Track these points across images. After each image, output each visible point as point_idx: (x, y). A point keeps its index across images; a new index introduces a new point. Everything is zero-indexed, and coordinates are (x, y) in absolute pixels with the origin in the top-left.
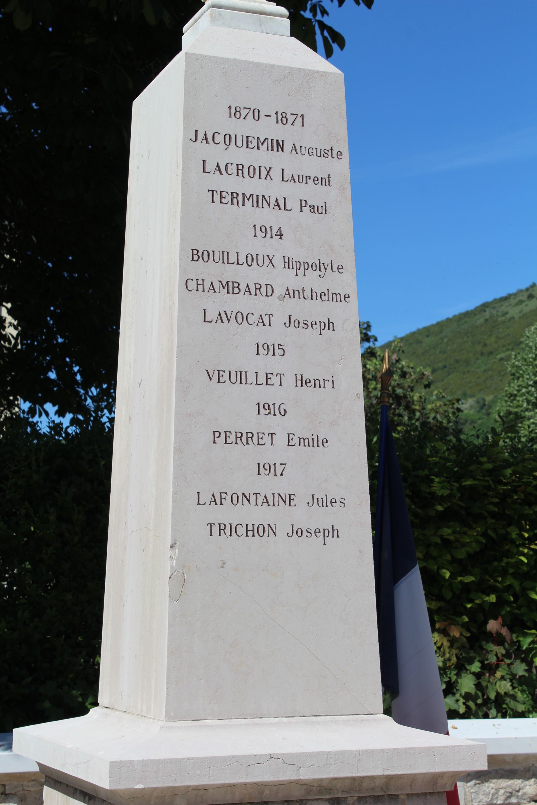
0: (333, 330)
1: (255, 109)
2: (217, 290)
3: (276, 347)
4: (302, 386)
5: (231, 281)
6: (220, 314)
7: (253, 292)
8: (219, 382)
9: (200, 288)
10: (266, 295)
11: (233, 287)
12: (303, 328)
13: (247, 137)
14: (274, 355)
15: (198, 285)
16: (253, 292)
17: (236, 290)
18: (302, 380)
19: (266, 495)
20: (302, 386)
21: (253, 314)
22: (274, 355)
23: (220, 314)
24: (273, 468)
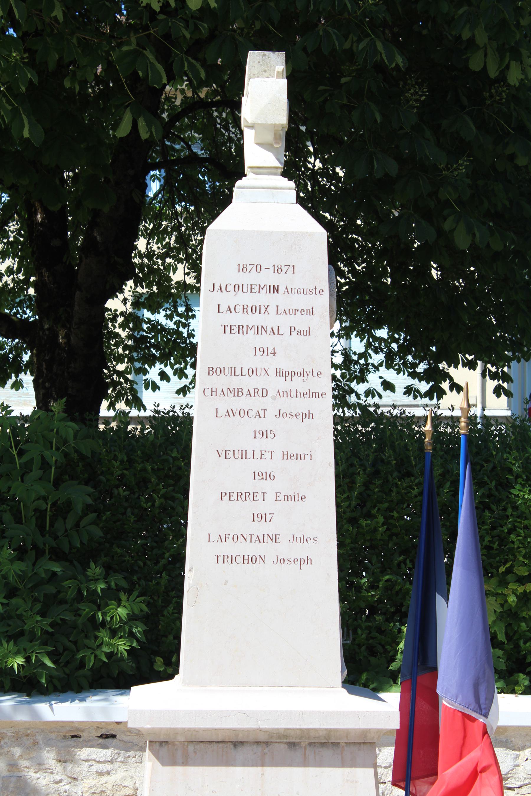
2: (226, 394)
4: (287, 459)
7: (252, 394)
9: (214, 393)
11: (238, 392)
16: (252, 394)
17: (240, 394)
18: (287, 455)
22: (267, 437)
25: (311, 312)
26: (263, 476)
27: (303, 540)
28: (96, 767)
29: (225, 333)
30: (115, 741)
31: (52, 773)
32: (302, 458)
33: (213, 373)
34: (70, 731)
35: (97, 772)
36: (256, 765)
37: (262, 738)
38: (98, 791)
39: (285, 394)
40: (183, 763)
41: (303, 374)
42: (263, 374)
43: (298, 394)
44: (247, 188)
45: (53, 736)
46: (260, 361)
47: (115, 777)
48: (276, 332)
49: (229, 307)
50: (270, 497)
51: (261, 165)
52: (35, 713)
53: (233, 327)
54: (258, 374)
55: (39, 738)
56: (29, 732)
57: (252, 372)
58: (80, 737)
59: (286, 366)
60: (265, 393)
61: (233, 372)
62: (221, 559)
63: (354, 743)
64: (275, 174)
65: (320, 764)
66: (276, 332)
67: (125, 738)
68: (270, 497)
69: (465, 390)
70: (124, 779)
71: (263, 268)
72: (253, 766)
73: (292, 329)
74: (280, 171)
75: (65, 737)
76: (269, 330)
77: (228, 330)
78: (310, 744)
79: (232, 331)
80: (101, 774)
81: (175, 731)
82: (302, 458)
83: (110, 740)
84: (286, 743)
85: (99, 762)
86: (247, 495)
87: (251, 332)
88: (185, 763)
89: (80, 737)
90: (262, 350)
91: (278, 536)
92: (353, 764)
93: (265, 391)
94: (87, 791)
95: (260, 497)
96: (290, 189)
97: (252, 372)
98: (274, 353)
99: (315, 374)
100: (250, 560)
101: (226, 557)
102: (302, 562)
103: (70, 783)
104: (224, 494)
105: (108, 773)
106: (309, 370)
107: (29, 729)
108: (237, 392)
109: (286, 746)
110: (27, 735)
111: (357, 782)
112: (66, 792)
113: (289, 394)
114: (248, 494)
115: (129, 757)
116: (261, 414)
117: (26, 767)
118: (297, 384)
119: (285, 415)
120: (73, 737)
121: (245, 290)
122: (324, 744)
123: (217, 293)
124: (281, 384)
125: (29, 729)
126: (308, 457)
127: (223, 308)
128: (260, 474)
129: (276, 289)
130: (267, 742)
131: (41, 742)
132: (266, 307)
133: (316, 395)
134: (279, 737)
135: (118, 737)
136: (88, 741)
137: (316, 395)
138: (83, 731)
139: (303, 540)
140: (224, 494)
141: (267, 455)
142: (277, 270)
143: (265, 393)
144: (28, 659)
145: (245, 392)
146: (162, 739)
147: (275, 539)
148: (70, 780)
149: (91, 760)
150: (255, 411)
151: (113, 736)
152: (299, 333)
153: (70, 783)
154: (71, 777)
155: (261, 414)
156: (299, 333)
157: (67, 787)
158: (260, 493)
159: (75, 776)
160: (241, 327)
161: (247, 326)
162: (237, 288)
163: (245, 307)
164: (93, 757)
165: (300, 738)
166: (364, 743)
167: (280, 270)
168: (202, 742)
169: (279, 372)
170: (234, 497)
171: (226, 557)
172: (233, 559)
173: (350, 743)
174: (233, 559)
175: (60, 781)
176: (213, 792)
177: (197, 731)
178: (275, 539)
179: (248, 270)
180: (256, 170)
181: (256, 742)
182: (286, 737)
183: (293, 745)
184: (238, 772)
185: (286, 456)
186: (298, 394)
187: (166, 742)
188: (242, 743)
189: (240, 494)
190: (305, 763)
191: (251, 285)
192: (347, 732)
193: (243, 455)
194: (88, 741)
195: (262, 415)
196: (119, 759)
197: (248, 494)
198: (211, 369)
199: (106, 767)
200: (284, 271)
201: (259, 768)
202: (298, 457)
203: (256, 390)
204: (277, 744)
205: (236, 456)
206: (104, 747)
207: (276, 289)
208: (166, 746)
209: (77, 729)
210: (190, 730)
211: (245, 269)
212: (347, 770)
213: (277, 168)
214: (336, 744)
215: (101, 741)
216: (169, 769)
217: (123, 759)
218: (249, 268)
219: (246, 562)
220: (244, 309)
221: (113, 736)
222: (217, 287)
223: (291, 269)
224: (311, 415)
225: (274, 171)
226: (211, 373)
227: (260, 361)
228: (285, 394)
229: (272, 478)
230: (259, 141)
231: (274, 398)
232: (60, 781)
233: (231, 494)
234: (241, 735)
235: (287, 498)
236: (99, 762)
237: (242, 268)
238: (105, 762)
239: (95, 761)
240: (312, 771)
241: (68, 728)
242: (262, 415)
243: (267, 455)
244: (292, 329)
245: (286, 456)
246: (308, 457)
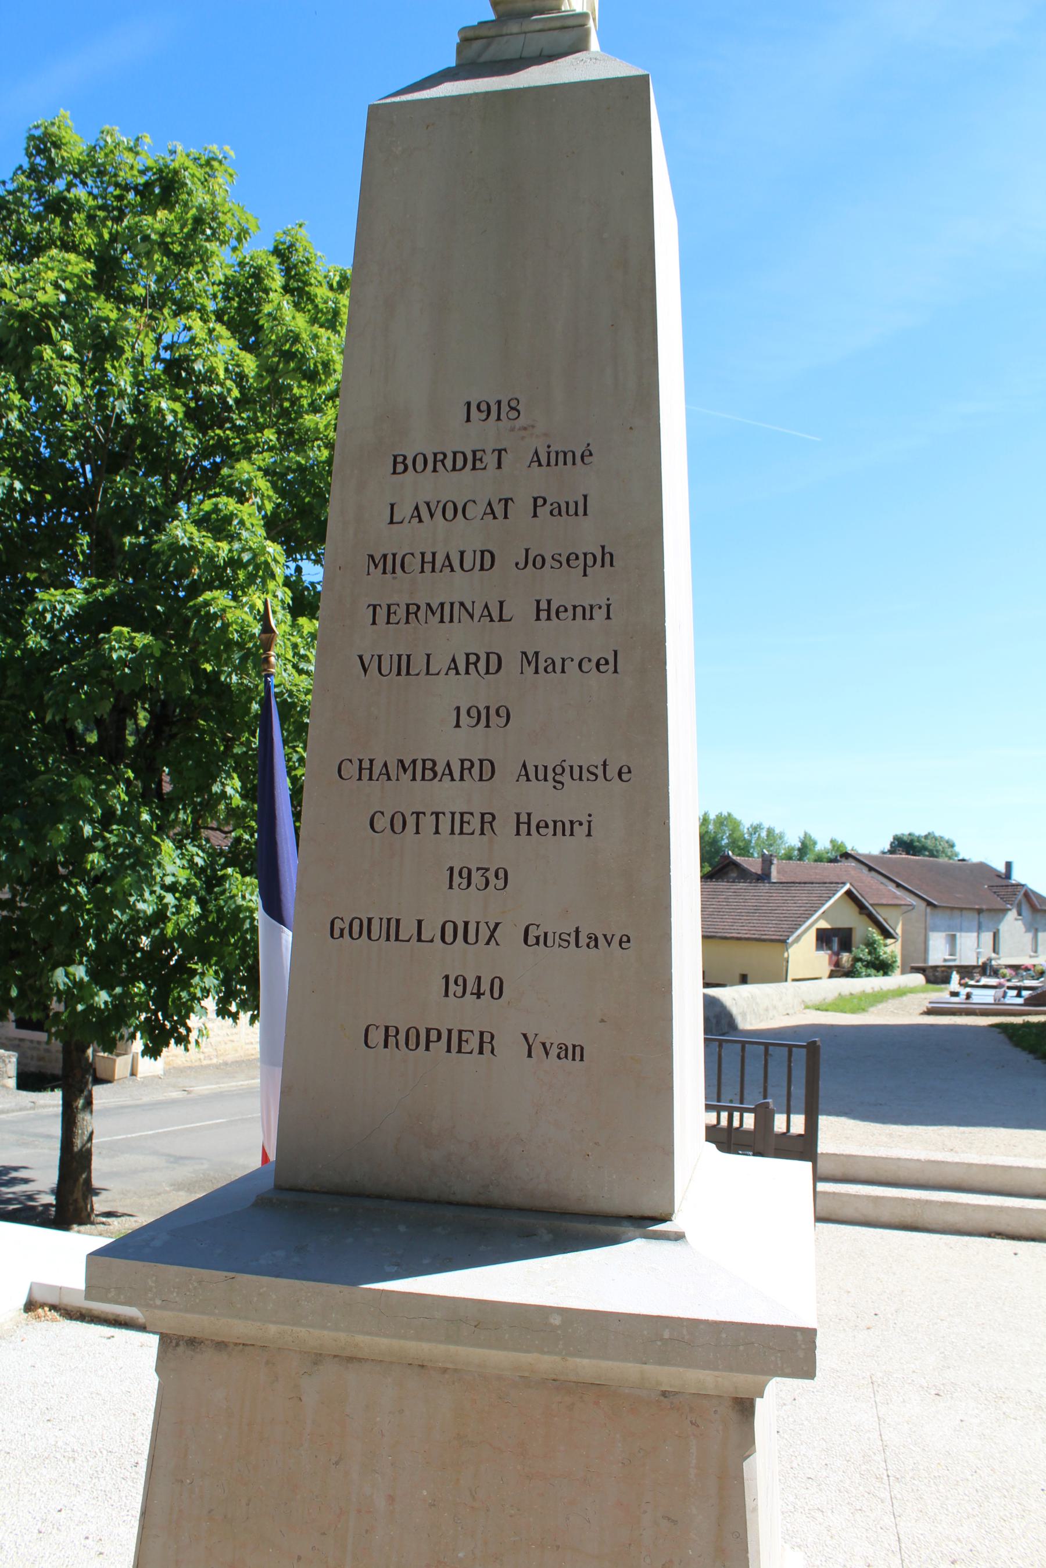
0: (582, 1059)
1: (462, 997)
2: (393, 777)
3: (492, 712)
4: (529, 834)
5: (420, 757)
6: (417, 508)
7: (462, 668)
8: (388, 622)
9: (366, 774)
10: (481, 779)
11: (424, 769)
12: (560, 555)
13: (462, 814)
14: (488, 726)
15: (361, 769)
16: (462, 668)
17: (429, 774)
18: (529, 824)
19: (450, 762)
20: (529, 834)
21: (474, 502)
22: (488, 726)
23: (417, 508)
24: (494, 409)
33: (406, 469)
69: (968, 1001)
93: (494, 659)
102: (590, 562)
126: (600, 615)
132: (492, 927)
150: (482, 507)
191: (460, 1032)
224: (607, 558)
226: (400, 468)
246: (600, 615)
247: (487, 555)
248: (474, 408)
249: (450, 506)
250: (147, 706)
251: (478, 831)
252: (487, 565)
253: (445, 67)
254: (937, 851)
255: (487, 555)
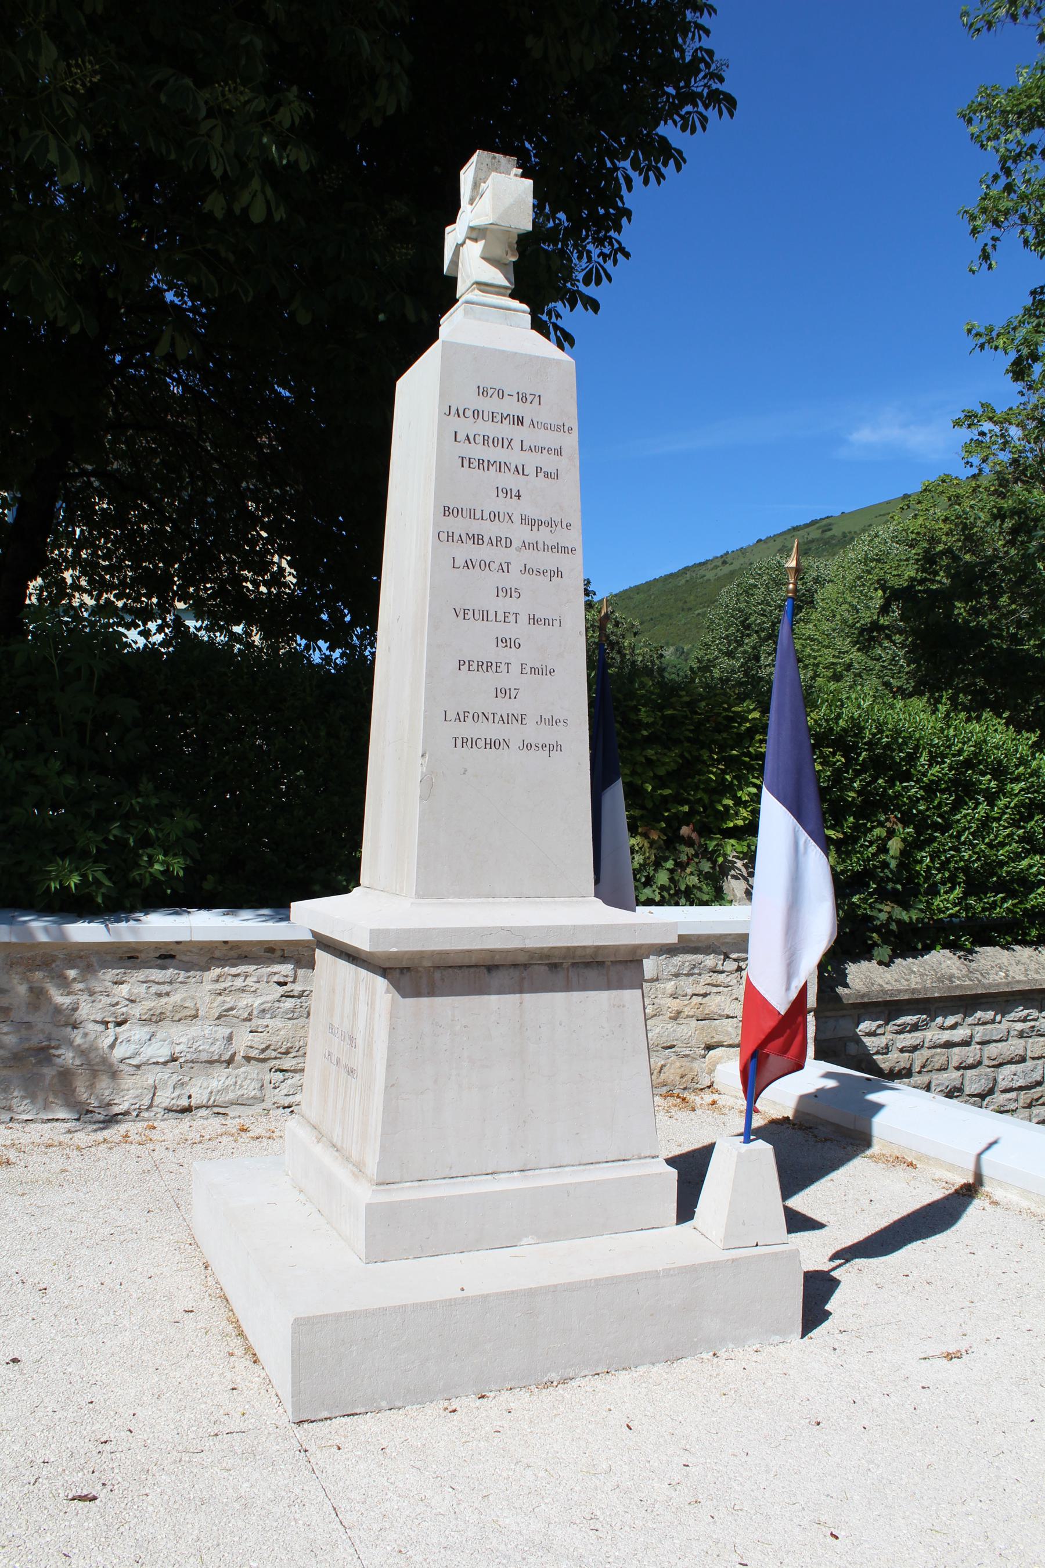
2: (464, 541)
7: (494, 543)
9: (450, 539)
16: (494, 543)
17: (481, 542)
25: (559, 452)
26: (506, 642)
27: (552, 722)
28: (155, 988)
29: (462, 466)
30: (175, 962)
31: (108, 996)
32: (551, 624)
34: (126, 952)
35: (156, 993)
36: (514, 993)
37: (522, 959)
38: (158, 1012)
39: (531, 545)
40: (429, 993)
41: (550, 524)
42: (506, 520)
43: (546, 547)
44: (477, 304)
45: (109, 958)
46: (502, 505)
47: (175, 998)
48: (521, 471)
49: (467, 436)
50: (515, 668)
51: (490, 282)
52: (63, 934)
53: (472, 460)
54: (501, 519)
55: (94, 960)
56: (82, 953)
57: (495, 516)
58: (137, 958)
59: (533, 513)
60: (509, 543)
61: (472, 514)
62: (459, 742)
63: (620, 962)
64: (504, 295)
65: (584, 988)
66: (521, 471)
67: (186, 959)
68: (515, 668)
70: (184, 1000)
71: (506, 394)
72: (510, 993)
73: (538, 470)
74: (509, 292)
75: (121, 958)
76: (513, 468)
77: (466, 463)
78: (574, 965)
79: (471, 466)
80: (160, 995)
81: (421, 954)
82: (551, 624)
83: (169, 961)
84: (547, 964)
85: (158, 983)
86: (489, 665)
87: (492, 469)
88: (431, 993)
89: (137, 958)
90: (505, 491)
91: (524, 716)
92: (620, 986)
94: (146, 1013)
95: (503, 668)
96: (524, 312)
97: (495, 516)
98: (519, 496)
99: (564, 526)
100: (492, 744)
101: (465, 740)
103: (127, 1006)
104: (462, 663)
105: (168, 994)
106: (557, 519)
107: (82, 950)
108: (477, 539)
109: (547, 968)
110: (81, 957)
111: (624, 1006)
112: (123, 1014)
113: (535, 546)
114: (489, 664)
115: (189, 977)
116: (505, 568)
117: (80, 990)
118: (543, 535)
119: (531, 571)
120: (130, 958)
121: (486, 418)
122: (587, 965)
123: (453, 418)
124: (521, 533)
125: (82, 950)
127: (461, 437)
128: (504, 641)
129: (520, 421)
130: (525, 965)
131: (95, 964)
133: (565, 550)
134: (541, 958)
135: (177, 957)
136: (147, 962)
137: (565, 550)
138: (140, 952)
139: (552, 722)
140: (462, 663)
141: (512, 618)
142: (522, 398)
143: (509, 543)
144: (84, 876)
145: (486, 539)
146: (404, 964)
147: (521, 719)
148: (127, 1003)
149: (150, 981)
150: (497, 564)
151: (172, 957)
152: (547, 475)
153: (127, 1006)
154: (128, 1000)
155: (505, 568)
156: (547, 475)
157: (124, 1010)
158: (503, 663)
159: (133, 998)
160: (481, 462)
161: (488, 461)
162: (477, 414)
163: (486, 438)
164: (153, 978)
165: (564, 958)
166: (631, 961)
167: (524, 399)
168: (450, 967)
169: (524, 520)
170: (474, 666)
171: (465, 740)
172: (474, 743)
173: (616, 962)
174: (474, 743)
175: (117, 1004)
176: (465, 1027)
177: (447, 953)
178: (521, 719)
179: (489, 395)
180: (482, 287)
181: (513, 965)
182: (548, 957)
183: (554, 967)
184: (494, 1001)
185: (533, 620)
186: (546, 547)
187: (408, 969)
188: (497, 967)
189: (480, 664)
190: (568, 988)
192: (616, 948)
193: (484, 616)
194: (147, 962)
195: (505, 569)
196: (179, 980)
197: (489, 664)
198: (447, 509)
199: (166, 988)
200: (529, 400)
201: (518, 996)
202: (547, 622)
203: (499, 539)
204: (536, 966)
205: (476, 617)
206: (164, 968)
207: (520, 421)
208: (409, 974)
209: (135, 950)
210: (440, 953)
211: (485, 393)
212: (613, 993)
213: (506, 288)
214: (601, 964)
215: (159, 962)
216: (411, 1001)
217: (183, 980)
218: (490, 392)
219: (488, 746)
220: (485, 439)
221: (172, 957)
222: (453, 411)
223: (537, 399)
225: (503, 291)
226: (447, 513)
227: (502, 505)
228: (531, 545)
229: (517, 646)
230: (487, 256)
231: (518, 549)
232: (117, 1004)
233: (471, 663)
234: (497, 957)
235: (534, 670)
236: (158, 983)
237: (483, 392)
238: (164, 983)
239: (154, 982)
240: (576, 996)
241: (125, 949)
242: (505, 569)
243: (512, 618)
244: (538, 470)
245: (533, 620)
246: (556, 623)
247: (508, 540)
248: (500, 490)
249: (483, 563)
250: (677, 54)
251: (512, 690)
252: (508, 545)
253: (594, 297)
254: (677, 650)
255: (508, 540)
